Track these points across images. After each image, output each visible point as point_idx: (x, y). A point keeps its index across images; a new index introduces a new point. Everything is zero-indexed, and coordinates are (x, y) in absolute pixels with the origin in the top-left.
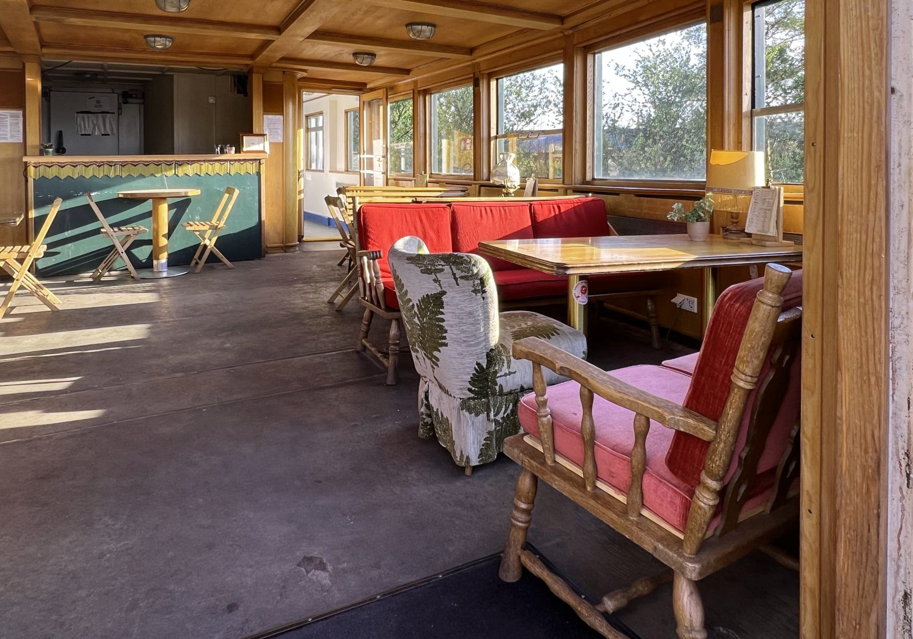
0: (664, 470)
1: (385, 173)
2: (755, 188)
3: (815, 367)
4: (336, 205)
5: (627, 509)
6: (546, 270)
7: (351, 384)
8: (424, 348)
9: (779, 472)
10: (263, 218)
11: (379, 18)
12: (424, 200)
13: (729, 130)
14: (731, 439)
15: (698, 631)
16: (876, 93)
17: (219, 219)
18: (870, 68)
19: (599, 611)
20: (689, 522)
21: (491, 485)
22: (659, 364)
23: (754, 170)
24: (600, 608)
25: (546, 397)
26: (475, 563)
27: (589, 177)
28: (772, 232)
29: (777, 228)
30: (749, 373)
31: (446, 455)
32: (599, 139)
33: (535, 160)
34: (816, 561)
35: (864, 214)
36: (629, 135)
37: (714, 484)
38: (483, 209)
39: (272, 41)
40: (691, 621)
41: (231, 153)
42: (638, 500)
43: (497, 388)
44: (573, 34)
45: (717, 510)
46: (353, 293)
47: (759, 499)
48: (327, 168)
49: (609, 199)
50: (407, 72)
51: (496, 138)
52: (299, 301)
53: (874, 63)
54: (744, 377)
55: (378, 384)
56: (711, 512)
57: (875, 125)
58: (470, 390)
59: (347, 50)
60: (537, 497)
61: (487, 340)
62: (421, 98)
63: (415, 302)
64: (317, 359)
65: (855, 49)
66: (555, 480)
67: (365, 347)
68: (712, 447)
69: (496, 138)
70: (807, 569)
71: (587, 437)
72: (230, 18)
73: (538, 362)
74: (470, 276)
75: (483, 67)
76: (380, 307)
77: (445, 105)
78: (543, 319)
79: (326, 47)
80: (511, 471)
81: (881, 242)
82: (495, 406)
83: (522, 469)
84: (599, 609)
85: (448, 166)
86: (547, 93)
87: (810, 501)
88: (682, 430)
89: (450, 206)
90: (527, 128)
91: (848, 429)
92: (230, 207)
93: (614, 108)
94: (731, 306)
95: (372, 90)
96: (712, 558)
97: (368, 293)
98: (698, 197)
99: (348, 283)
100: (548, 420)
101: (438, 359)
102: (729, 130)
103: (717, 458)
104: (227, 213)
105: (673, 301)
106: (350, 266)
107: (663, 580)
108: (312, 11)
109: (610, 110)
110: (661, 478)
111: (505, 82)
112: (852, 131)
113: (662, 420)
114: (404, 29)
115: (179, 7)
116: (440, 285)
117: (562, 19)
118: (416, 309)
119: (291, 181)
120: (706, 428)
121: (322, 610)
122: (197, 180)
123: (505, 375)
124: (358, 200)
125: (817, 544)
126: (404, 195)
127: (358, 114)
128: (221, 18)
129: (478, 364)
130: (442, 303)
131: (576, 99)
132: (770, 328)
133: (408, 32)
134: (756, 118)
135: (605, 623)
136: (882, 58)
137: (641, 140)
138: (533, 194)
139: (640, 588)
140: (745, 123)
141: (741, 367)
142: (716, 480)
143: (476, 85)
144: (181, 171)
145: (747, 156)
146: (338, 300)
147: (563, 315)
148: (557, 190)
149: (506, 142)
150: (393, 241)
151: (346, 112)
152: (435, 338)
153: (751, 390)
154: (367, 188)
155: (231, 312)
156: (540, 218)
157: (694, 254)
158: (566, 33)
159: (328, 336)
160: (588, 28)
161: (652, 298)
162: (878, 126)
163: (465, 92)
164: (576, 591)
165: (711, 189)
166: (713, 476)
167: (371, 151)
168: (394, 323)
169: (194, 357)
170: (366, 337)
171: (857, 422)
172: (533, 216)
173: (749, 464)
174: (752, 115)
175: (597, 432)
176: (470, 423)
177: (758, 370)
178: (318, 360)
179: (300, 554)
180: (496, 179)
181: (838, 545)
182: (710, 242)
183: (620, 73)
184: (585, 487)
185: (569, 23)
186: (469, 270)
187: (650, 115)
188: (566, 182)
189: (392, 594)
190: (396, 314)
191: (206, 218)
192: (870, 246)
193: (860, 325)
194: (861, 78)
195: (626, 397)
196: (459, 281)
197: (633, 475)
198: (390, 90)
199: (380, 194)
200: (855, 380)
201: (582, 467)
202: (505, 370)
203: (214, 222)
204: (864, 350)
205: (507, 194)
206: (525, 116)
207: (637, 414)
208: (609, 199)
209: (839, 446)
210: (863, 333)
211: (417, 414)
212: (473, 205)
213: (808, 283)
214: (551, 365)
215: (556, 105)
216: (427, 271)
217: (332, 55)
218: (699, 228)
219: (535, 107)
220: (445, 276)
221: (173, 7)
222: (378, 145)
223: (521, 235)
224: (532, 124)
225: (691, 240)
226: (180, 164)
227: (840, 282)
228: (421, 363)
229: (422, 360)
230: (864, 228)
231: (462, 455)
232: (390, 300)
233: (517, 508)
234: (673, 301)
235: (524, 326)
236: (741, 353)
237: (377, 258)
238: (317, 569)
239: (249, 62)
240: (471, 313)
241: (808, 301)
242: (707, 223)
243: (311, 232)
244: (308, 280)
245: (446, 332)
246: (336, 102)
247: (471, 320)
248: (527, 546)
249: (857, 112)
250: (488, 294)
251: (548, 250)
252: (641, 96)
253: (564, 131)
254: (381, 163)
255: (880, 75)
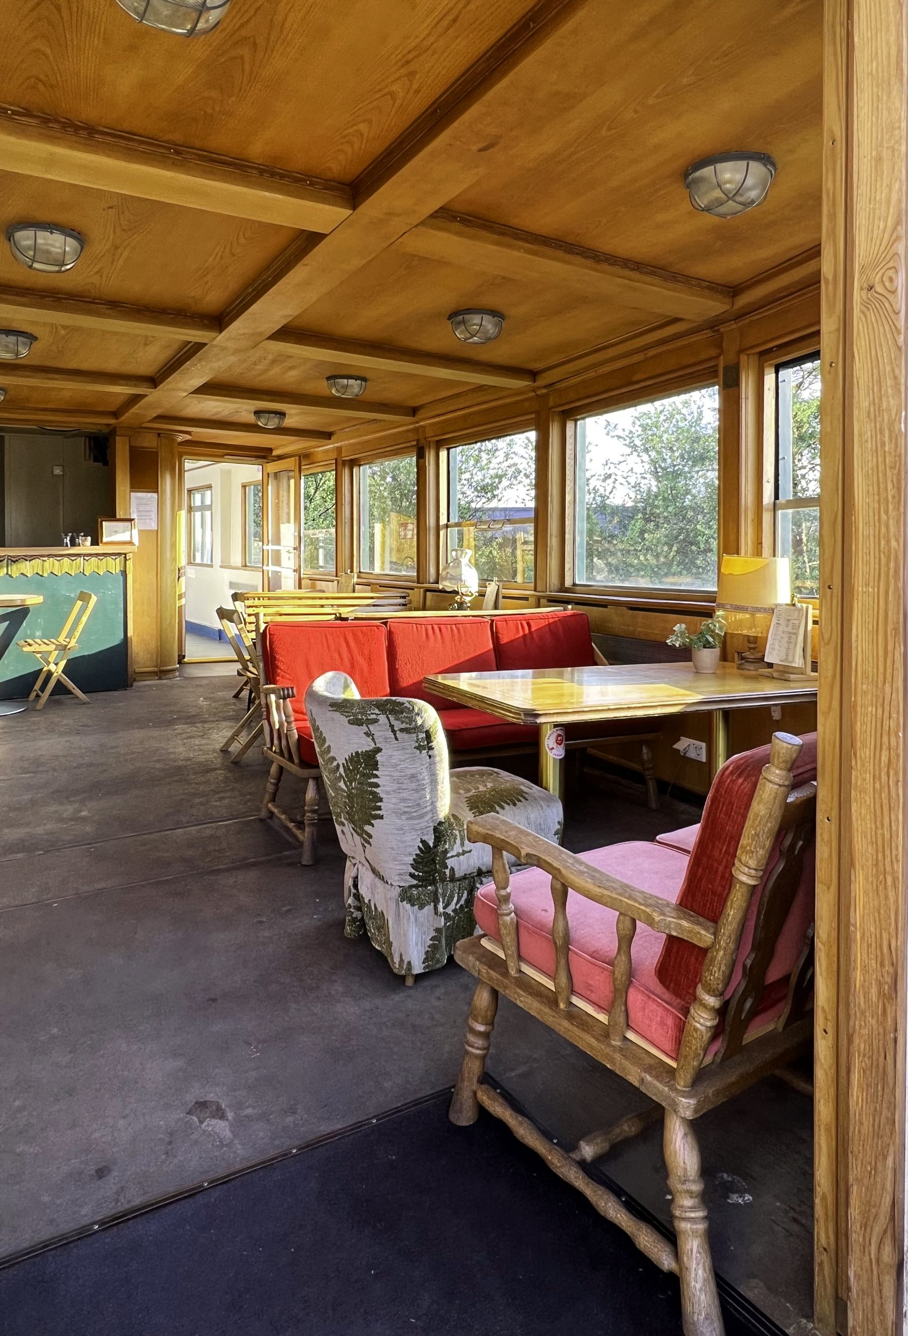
0: (654, 983)
1: (298, 570)
2: (777, 605)
3: (831, 855)
4: (232, 621)
5: (608, 1032)
6: (511, 718)
7: (254, 865)
8: (351, 821)
9: (794, 980)
10: (130, 633)
11: (291, 368)
12: (351, 616)
13: (746, 534)
14: (732, 946)
15: (694, 1181)
16: (893, 543)
17: (70, 635)
18: (887, 512)
19: (574, 1160)
20: (682, 1047)
21: (439, 999)
22: (652, 839)
23: (776, 583)
24: (575, 1156)
25: (508, 890)
26: (416, 1103)
27: (568, 583)
28: (798, 662)
29: (804, 658)
30: (753, 866)
31: (381, 960)
32: (581, 533)
33: (500, 549)
34: (832, 1091)
35: (880, 684)
36: (625, 515)
37: (712, 1001)
38: (430, 627)
39: (146, 396)
40: (686, 1169)
41: (86, 545)
42: (622, 1020)
43: (447, 872)
44: (547, 394)
45: (717, 1032)
46: (255, 737)
47: (770, 1013)
48: (217, 561)
49: (594, 612)
50: (328, 435)
51: (447, 526)
52: (181, 749)
53: (891, 507)
54: (747, 871)
55: (291, 865)
56: (709, 1034)
57: (892, 581)
58: (412, 875)
59: (245, 407)
60: (499, 1013)
61: (434, 810)
62: (346, 472)
63: (341, 761)
64: (208, 830)
65: (871, 488)
66: (519, 996)
67: (272, 813)
68: (709, 955)
69: (447, 526)
70: (822, 1102)
71: (559, 942)
72: (85, 366)
73: (499, 847)
74: (412, 729)
75: (429, 433)
76: (293, 762)
77: (379, 479)
78: (508, 779)
79: (218, 403)
80: (464, 980)
81: (898, 718)
82: (444, 896)
83: (477, 981)
84: (574, 1156)
85: (383, 563)
86: (516, 459)
87: (826, 1019)
88: (674, 934)
89: (385, 623)
90: (487, 506)
91: (862, 938)
92: (84, 619)
93: (604, 480)
94: (733, 781)
95: (280, 458)
96: (710, 1092)
97: (276, 742)
98: (708, 614)
99: (247, 724)
100: (512, 919)
101: (370, 836)
102: (746, 534)
103: (715, 969)
104: (80, 627)
105: (675, 746)
106: (249, 701)
107: (653, 1119)
108: (200, 360)
109: (600, 483)
110: (649, 993)
111: (457, 451)
112: (867, 585)
113: (650, 922)
114: (325, 383)
115: (17, 353)
116: (373, 739)
117: (533, 375)
118: (341, 770)
119: (169, 582)
120: (703, 932)
121: (221, 1172)
122: (38, 583)
123: (458, 855)
124: (262, 619)
125: (833, 1071)
126: (322, 610)
127: (261, 489)
128: (73, 365)
129: (423, 842)
130: (376, 763)
131: (551, 475)
132: (777, 812)
133: (330, 387)
134: (780, 513)
135: (581, 1174)
136: (899, 502)
137: (638, 523)
138: (496, 607)
139: (626, 1127)
140: (767, 517)
141: (743, 859)
142: (715, 996)
143: (421, 456)
144: (15, 570)
145: (768, 565)
146: (235, 748)
147: (534, 775)
148: (526, 599)
149: (461, 534)
150: (312, 678)
151: (244, 487)
152: (366, 809)
153: (754, 886)
154: (271, 594)
155: (91, 765)
156: (505, 639)
157: (699, 693)
158: (539, 392)
159: (221, 799)
160: (567, 388)
161: (648, 743)
162: (896, 582)
163: (409, 462)
164: (547, 1135)
165: (722, 606)
166: (711, 992)
167: (277, 541)
168: (311, 785)
169: (40, 830)
170: (273, 800)
171: (872, 929)
172: (495, 637)
173: (755, 975)
174: (775, 508)
175: (572, 934)
176: (412, 919)
177: (764, 862)
178: (208, 832)
179: (190, 1098)
180: (447, 583)
181: (852, 1076)
182: (720, 676)
183: (612, 434)
184: (557, 1005)
185: (542, 381)
186: (411, 720)
187: (649, 490)
188: (538, 589)
189: (310, 1147)
190: (313, 772)
191: (51, 633)
192: (886, 723)
193: (875, 815)
194: (877, 524)
195: (606, 892)
196: (399, 734)
197: (616, 990)
198: (304, 457)
199: (294, 607)
200: (870, 880)
201: (553, 978)
202: (457, 848)
203: (62, 639)
204: (880, 843)
205: (461, 606)
206: (485, 489)
207: (621, 914)
208: (594, 612)
209: (853, 958)
210: (878, 824)
211: (342, 906)
212: (418, 623)
213: (824, 759)
214: (515, 851)
215: (527, 476)
216: (357, 722)
217: (226, 413)
218: (708, 657)
219: (500, 477)
220: (381, 730)
221: (7, 352)
222: (288, 531)
223: (476, 665)
224: (495, 500)
225: (697, 672)
226: (14, 560)
227: (853, 763)
228: (348, 839)
229: (349, 836)
230: (880, 701)
231: (401, 960)
232: (306, 753)
233: (472, 1031)
234: (675, 746)
235: (482, 788)
236: (744, 841)
237: (289, 696)
238: (213, 1117)
239: (112, 421)
240: (413, 776)
241: (823, 775)
242: (717, 651)
243: (195, 649)
244: (192, 719)
245: (381, 800)
246: (230, 472)
247: (413, 786)
248: (486, 1079)
249: (872, 563)
250: (435, 752)
251: (513, 691)
252: (639, 464)
253: (536, 510)
254: (292, 556)
255: (898, 522)
